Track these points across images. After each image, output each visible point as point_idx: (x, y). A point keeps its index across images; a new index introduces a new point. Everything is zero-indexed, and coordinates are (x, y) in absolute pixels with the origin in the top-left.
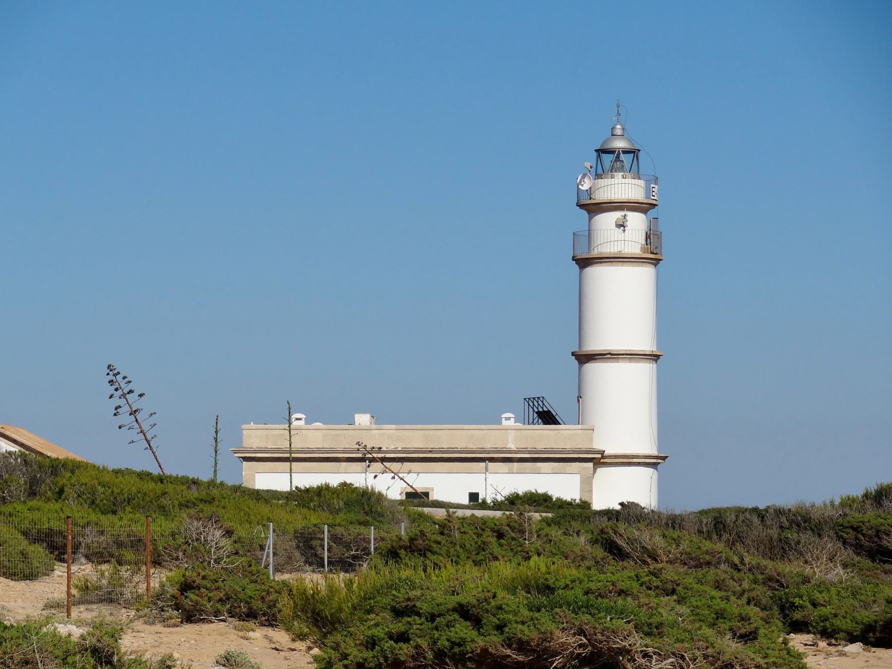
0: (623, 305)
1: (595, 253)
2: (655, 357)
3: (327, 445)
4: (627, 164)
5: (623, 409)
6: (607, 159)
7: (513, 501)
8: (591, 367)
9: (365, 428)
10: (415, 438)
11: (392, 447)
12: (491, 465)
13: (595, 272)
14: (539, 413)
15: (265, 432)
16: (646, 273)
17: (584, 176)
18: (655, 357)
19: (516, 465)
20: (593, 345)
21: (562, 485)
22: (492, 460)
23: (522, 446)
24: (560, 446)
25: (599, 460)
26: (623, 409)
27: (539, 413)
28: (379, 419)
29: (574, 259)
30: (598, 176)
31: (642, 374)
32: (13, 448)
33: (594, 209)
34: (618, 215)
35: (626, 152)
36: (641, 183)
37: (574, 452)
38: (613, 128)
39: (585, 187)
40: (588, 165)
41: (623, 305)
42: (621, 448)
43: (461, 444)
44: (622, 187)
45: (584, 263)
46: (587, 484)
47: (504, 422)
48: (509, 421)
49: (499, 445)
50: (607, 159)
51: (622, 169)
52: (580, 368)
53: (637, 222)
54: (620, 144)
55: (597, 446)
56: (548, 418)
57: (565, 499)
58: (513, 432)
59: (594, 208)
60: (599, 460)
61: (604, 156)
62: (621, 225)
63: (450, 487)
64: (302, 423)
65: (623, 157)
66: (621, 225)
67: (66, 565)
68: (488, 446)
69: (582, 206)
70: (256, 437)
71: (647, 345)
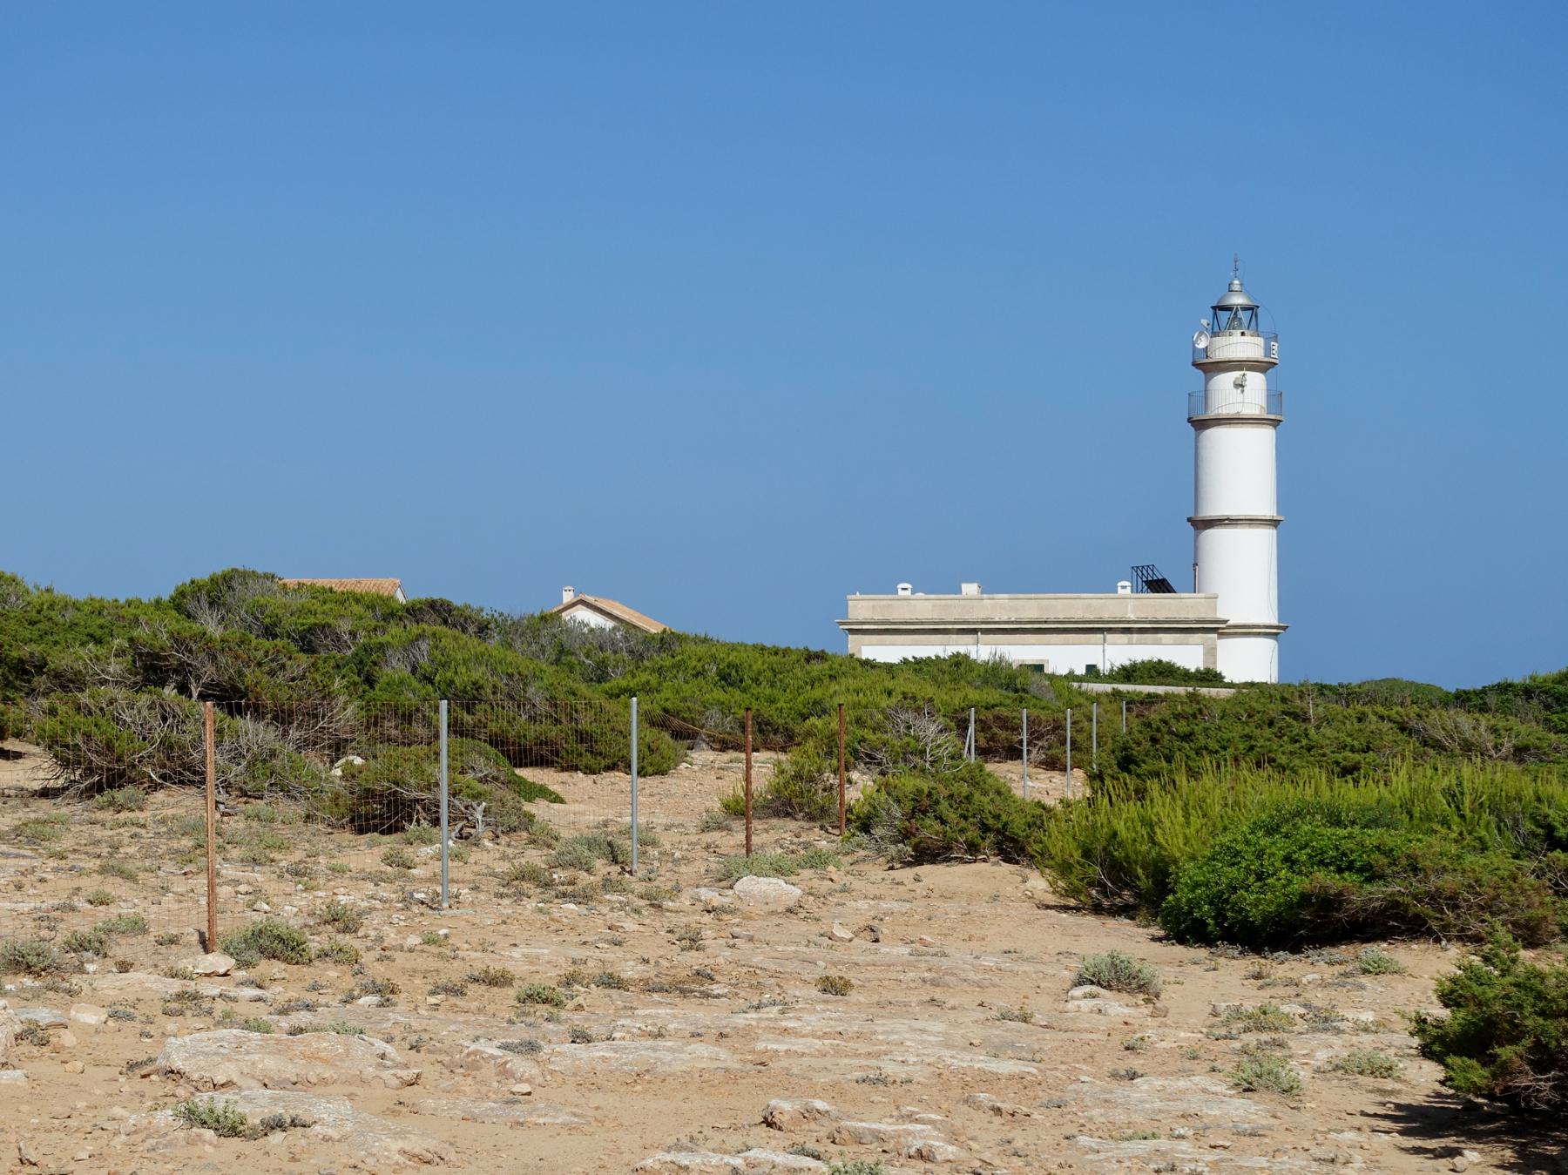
0: (1242, 469)
1: (1212, 414)
2: (1274, 523)
3: (936, 616)
4: (1245, 321)
5: (1243, 576)
6: (1223, 316)
7: (1129, 673)
8: (1210, 534)
9: (972, 601)
10: (1029, 607)
11: (1005, 618)
12: (1109, 637)
13: (1214, 434)
14: (1147, 582)
15: (872, 603)
16: (1267, 435)
17: (1201, 333)
18: (1274, 523)
19: (1135, 636)
20: (1209, 512)
21: (1187, 655)
22: (1110, 630)
23: (1142, 615)
24: (1182, 615)
25: (1217, 629)
26: (1243, 576)
27: (1147, 582)
28: (987, 589)
29: (1190, 420)
30: (1214, 334)
31: (1265, 538)
32: (610, 624)
33: (1211, 368)
34: (1237, 374)
35: (1245, 309)
36: (1260, 341)
37: (1198, 622)
38: (1230, 284)
39: (1201, 345)
40: (1204, 322)
41: (1242, 469)
42: (1240, 617)
43: (1078, 615)
44: (1241, 345)
45: (1201, 425)
46: (1211, 652)
47: (901, 593)
48: (1124, 588)
49: (1119, 615)
50: (1224, 316)
51: (1240, 326)
52: (1196, 537)
53: (1256, 380)
54: (1238, 300)
55: (1221, 615)
56: (1159, 586)
57: (1445, 688)
58: (1129, 602)
59: (1211, 368)
60: (1217, 629)
61: (1220, 313)
62: (1240, 385)
63: (1064, 658)
64: (908, 593)
65: (1241, 314)
66: (1240, 385)
67: (743, 756)
68: (1106, 616)
69: (1195, 365)
70: (861, 608)
71: (1269, 512)
